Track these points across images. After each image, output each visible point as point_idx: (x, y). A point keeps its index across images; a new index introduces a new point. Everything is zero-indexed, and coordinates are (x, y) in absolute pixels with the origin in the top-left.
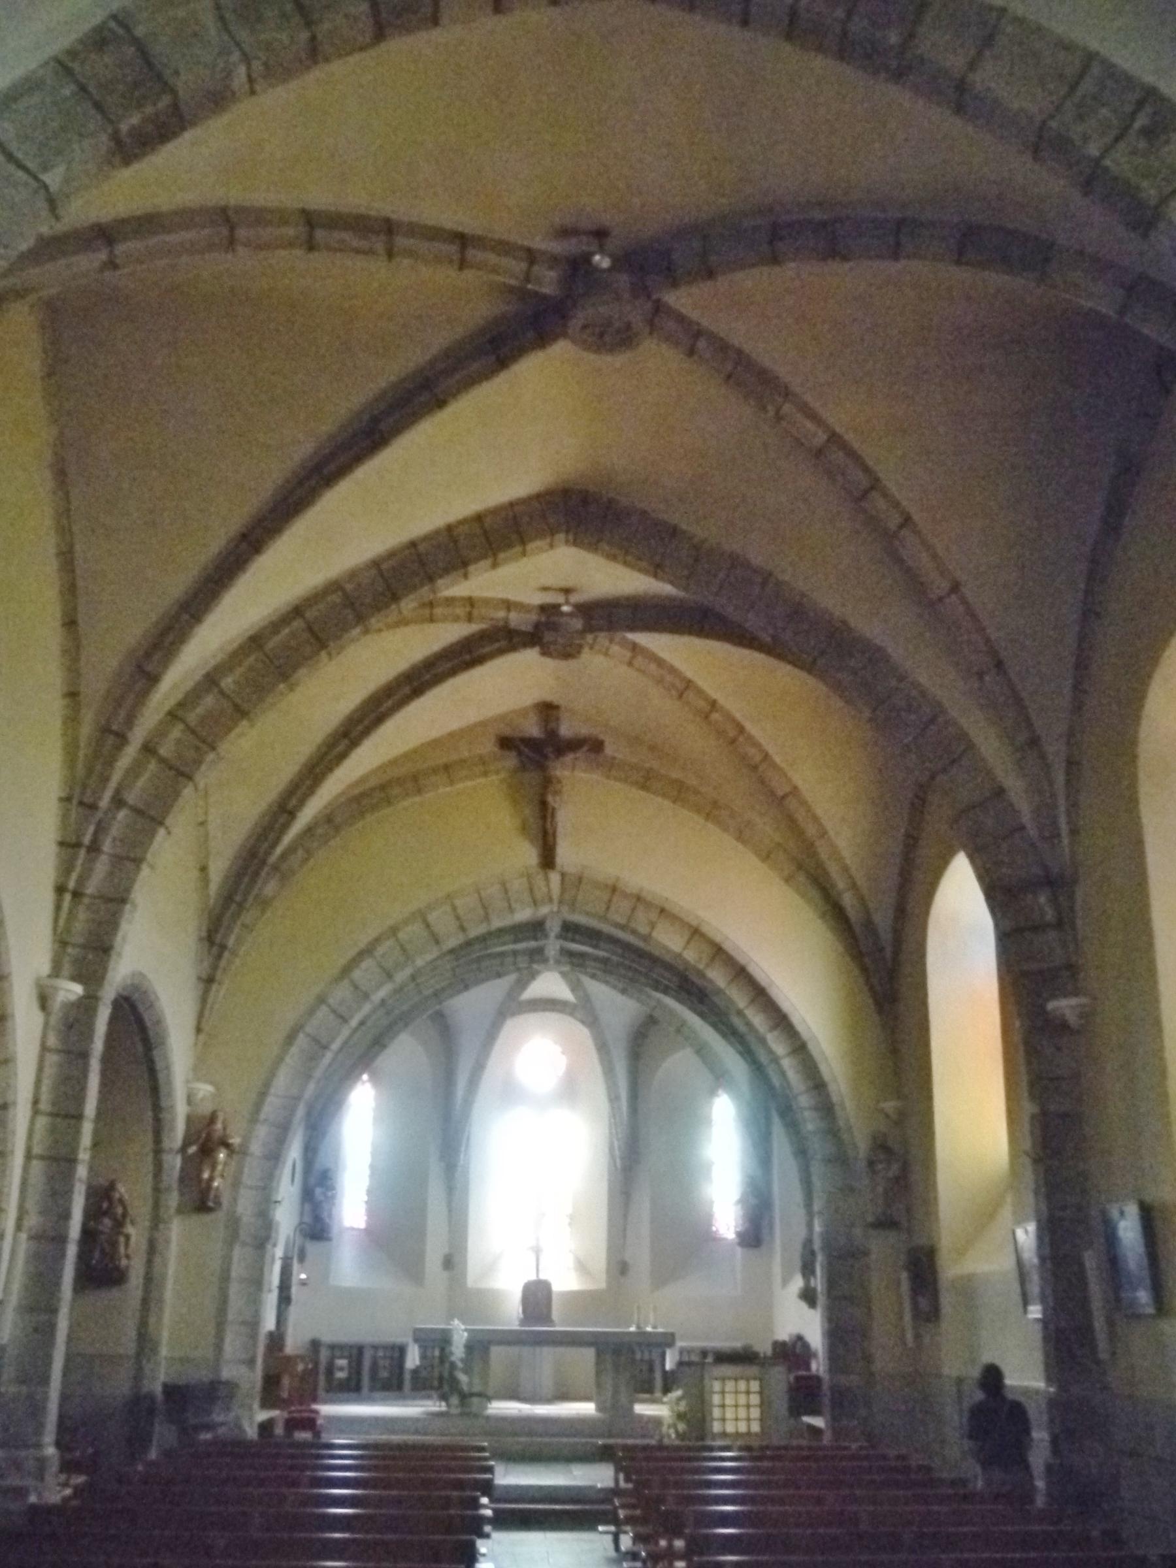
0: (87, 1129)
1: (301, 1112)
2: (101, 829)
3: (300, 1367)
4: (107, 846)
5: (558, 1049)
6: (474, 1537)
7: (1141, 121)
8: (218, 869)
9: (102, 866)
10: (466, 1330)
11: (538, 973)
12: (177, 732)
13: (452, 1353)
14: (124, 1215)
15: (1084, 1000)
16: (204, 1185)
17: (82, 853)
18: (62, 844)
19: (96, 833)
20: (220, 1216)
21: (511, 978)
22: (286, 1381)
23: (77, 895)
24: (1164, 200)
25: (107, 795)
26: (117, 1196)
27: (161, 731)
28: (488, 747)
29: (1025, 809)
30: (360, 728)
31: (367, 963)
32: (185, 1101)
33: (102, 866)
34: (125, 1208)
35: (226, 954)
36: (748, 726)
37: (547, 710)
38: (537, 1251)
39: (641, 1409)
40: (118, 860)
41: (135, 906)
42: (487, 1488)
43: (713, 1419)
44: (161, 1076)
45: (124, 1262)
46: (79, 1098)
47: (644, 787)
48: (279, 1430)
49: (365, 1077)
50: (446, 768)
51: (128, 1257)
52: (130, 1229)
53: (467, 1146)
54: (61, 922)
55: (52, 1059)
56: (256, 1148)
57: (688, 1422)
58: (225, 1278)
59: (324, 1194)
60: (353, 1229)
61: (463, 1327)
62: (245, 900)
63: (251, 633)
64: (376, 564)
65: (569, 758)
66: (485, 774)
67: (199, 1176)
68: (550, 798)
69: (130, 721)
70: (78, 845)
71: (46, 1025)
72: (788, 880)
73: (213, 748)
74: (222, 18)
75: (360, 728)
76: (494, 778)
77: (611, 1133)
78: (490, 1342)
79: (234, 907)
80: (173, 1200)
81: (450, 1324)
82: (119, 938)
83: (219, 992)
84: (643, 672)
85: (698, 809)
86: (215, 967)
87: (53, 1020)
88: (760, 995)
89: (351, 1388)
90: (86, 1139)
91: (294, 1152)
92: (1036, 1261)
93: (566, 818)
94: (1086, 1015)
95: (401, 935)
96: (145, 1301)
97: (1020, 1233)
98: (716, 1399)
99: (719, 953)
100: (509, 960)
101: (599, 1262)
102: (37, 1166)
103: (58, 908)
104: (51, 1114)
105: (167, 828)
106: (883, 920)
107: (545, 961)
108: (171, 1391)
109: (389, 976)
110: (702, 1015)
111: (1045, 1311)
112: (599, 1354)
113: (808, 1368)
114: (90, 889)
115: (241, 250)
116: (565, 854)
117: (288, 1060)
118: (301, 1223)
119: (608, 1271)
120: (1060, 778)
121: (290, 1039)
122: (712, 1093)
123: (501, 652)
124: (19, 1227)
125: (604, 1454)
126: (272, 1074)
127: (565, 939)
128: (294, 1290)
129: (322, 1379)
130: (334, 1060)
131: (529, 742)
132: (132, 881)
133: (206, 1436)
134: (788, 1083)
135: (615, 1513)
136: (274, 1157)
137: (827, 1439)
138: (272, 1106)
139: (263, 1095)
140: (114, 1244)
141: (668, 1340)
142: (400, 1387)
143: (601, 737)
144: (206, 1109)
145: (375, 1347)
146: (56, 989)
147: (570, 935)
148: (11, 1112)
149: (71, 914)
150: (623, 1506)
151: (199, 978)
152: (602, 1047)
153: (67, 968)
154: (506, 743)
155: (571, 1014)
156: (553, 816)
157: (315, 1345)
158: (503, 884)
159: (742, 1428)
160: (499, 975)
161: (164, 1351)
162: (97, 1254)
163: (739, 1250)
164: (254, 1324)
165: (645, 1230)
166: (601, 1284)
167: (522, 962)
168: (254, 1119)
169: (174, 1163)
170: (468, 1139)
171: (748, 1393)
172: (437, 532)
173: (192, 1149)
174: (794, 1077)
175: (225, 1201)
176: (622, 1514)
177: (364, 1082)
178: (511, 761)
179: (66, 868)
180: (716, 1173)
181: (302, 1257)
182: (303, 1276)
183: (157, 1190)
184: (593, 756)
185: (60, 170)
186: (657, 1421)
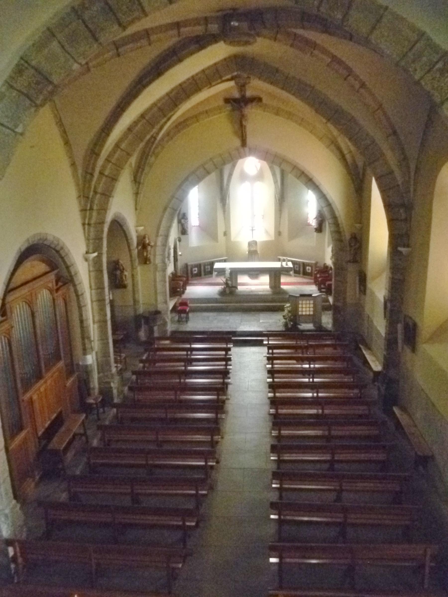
2: (92, 202)
4: (95, 207)
7: (440, 65)
9: (94, 214)
23: (89, 224)
24: (442, 103)
26: (120, 264)
27: (104, 167)
28: (221, 102)
29: (400, 180)
33: (94, 214)
40: (99, 211)
43: (299, 308)
44: (127, 232)
45: (126, 282)
46: (102, 283)
50: (207, 112)
53: (229, 197)
56: (159, 243)
58: (155, 281)
63: (128, 127)
64: (168, 94)
65: (249, 106)
66: (220, 113)
67: (143, 255)
69: (93, 169)
70: (86, 210)
71: (89, 265)
72: (328, 147)
74: (63, 47)
79: (141, 170)
80: (137, 262)
83: (141, 196)
85: (296, 122)
86: (138, 188)
87: (91, 263)
93: (249, 127)
101: (272, 231)
102: (95, 304)
103: (84, 229)
114: (93, 222)
115: (92, 69)
117: (165, 216)
119: (275, 234)
120: (412, 174)
121: (165, 209)
126: (161, 222)
131: (235, 101)
143: (261, 96)
144: (143, 234)
148: (85, 295)
149: (89, 232)
151: (134, 194)
154: (227, 101)
161: (141, 302)
162: (118, 281)
165: (287, 222)
168: (157, 236)
170: (229, 195)
171: (310, 304)
172: (188, 79)
173: (140, 247)
175: (152, 260)
179: (84, 218)
181: (180, 241)
183: (131, 261)
184: (260, 104)
185: (21, 125)
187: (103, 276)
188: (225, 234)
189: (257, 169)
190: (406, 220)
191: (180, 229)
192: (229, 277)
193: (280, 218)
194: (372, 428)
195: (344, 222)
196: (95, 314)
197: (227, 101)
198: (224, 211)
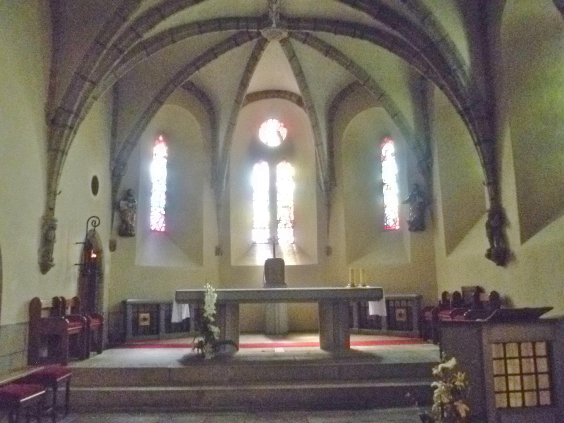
5: (260, 130)
10: (216, 292)
13: (204, 311)
61: (214, 290)
81: (203, 288)
130: (108, 54)
177: (160, 142)
188: (218, 251)
189: (281, 137)
191: (116, 223)
192: (214, 315)
193: (328, 219)
194: (76, 323)
198: (280, 357)
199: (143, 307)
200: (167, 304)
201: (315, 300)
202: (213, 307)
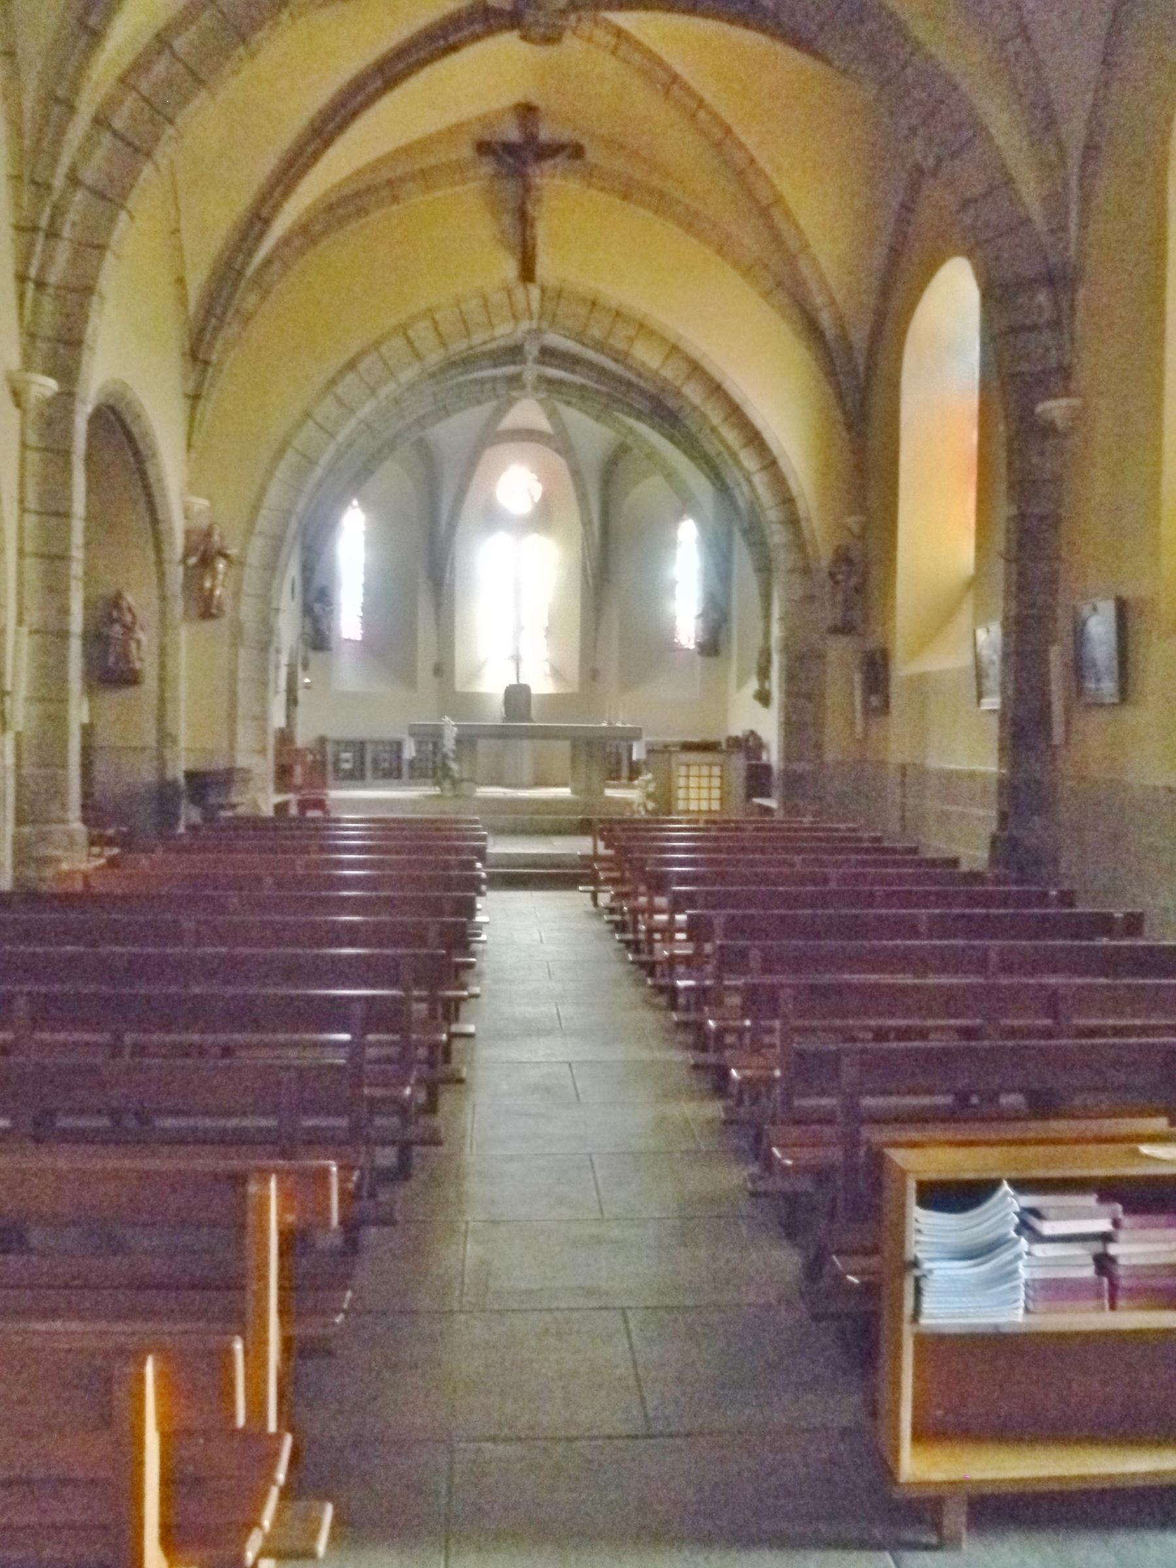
0: (78, 526)
1: (293, 525)
2: (58, 211)
3: (310, 758)
6: (473, 894)
8: (197, 279)
9: (63, 252)
11: (516, 399)
12: (130, 101)
13: (444, 746)
14: (134, 623)
15: (1075, 402)
16: (207, 593)
17: (40, 239)
18: (19, 229)
19: (53, 218)
20: (224, 621)
21: (488, 407)
22: (298, 770)
23: (40, 285)
25: (62, 170)
26: (124, 605)
28: (467, 151)
30: (331, 125)
31: (350, 378)
32: (182, 516)
33: (63, 252)
34: (134, 616)
35: (210, 370)
36: (736, 130)
37: (527, 112)
38: (517, 660)
39: (609, 792)
41: (102, 298)
42: (481, 854)
45: (138, 665)
47: (625, 197)
48: (293, 811)
49: (355, 502)
51: (141, 659)
52: (141, 636)
54: (27, 313)
55: (33, 457)
57: (655, 800)
59: (324, 610)
60: (349, 640)
62: (224, 313)
65: (547, 165)
66: (464, 182)
67: (201, 588)
68: (529, 207)
70: (35, 229)
72: (767, 295)
73: (171, 122)
75: (331, 125)
76: (471, 185)
77: (584, 555)
78: (478, 736)
80: (178, 607)
82: (90, 330)
83: (206, 409)
84: (625, 60)
86: (200, 384)
87: (32, 416)
88: (736, 413)
89: (356, 776)
90: (78, 537)
91: (293, 571)
92: (996, 658)
94: (1077, 416)
95: (383, 349)
96: (162, 700)
97: (982, 635)
98: (682, 782)
99: (696, 369)
100: (488, 386)
103: (21, 296)
104: (39, 513)
105: (129, 212)
106: (859, 337)
107: (523, 387)
108: (190, 776)
109: (373, 391)
110: (672, 439)
111: (1003, 704)
112: (574, 747)
113: (759, 758)
116: (545, 267)
118: (303, 634)
121: (281, 452)
122: (678, 517)
123: (476, 38)
124: (20, 622)
125: (584, 828)
126: (263, 490)
127: (543, 363)
128: (301, 694)
129: (330, 768)
131: (510, 148)
132: (98, 269)
133: (227, 814)
134: (757, 498)
135: (596, 873)
136: (272, 567)
137: (779, 815)
138: (266, 519)
139: (256, 508)
140: (125, 645)
141: (635, 734)
142: (399, 776)
144: (204, 522)
145: (376, 743)
146: (28, 383)
147: (547, 359)
149: (37, 303)
150: (604, 869)
152: (576, 473)
153: (38, 360)
154: (484, 148)
155: (547, 444)
156: (532, 226)
157: (322, 741)
158: (485, 299)
159: (704, 806)
160: (479, 402)
163: (699, 659)
164: (262, 718)
166: (574, 688)
167: (501, 389)
168: (249, 532)
169: (176, 575)
171: (710, 776)
173: (193, 561)
174: (766, 496)
175: (228, 607)
176: (602, 876)
177: (354, 508)
178: (487, 167)
179: (25, 257)
180: (679, 591)
181: (306, 666)
182: (307, 680)
183: (163, 598)
186: (628, 803)
187: (67, 484)
188: (438, 670)
189: (532, 497)
190: (1055, 325)
192: (454, 751)
195: (813, 514)
196: (28, 601)
197: (484, 148)
198: (438, 605)
199: (348, 744)
200: (391, 743)
201: (566, 738)
202: (453, 742)
